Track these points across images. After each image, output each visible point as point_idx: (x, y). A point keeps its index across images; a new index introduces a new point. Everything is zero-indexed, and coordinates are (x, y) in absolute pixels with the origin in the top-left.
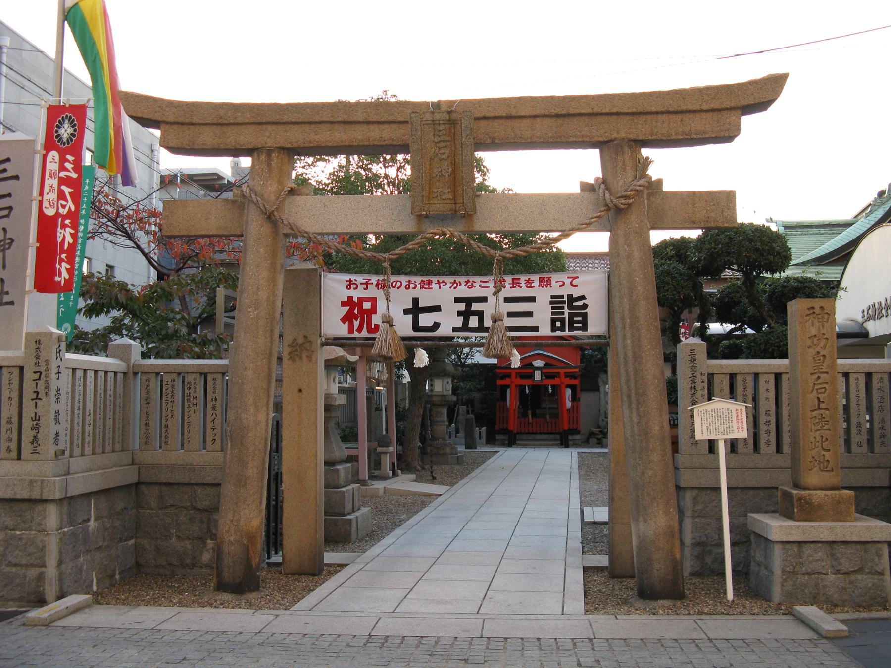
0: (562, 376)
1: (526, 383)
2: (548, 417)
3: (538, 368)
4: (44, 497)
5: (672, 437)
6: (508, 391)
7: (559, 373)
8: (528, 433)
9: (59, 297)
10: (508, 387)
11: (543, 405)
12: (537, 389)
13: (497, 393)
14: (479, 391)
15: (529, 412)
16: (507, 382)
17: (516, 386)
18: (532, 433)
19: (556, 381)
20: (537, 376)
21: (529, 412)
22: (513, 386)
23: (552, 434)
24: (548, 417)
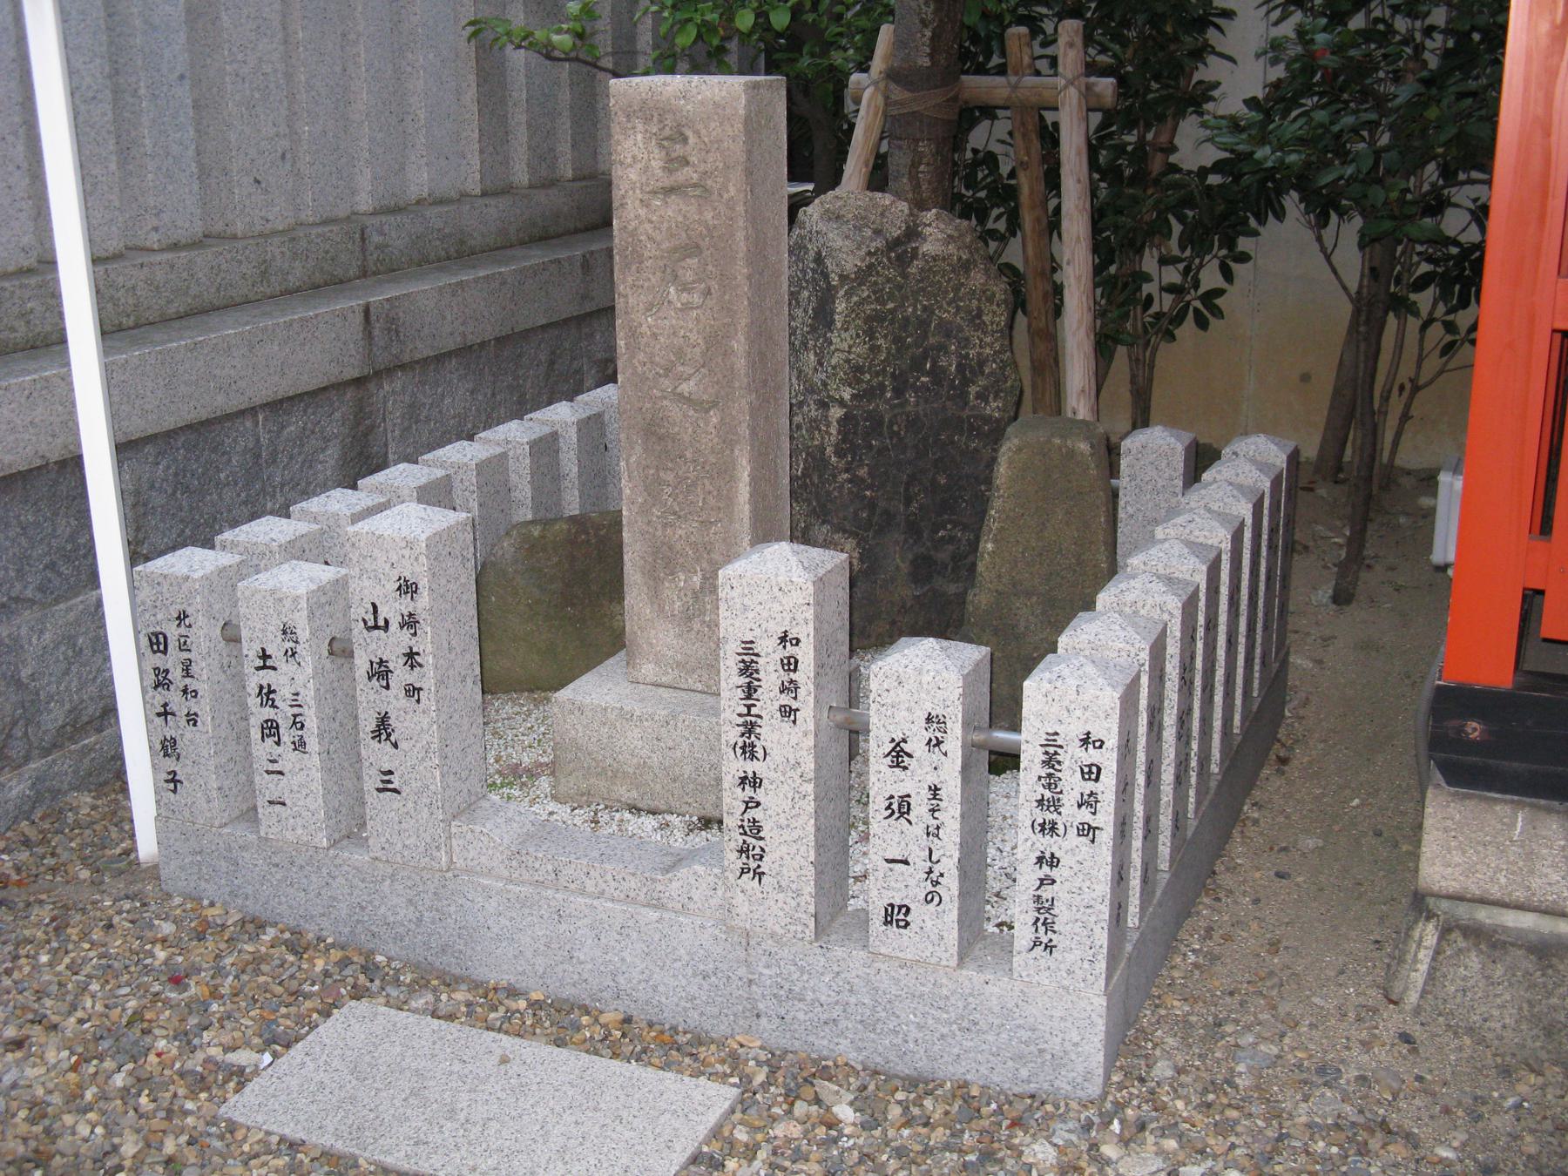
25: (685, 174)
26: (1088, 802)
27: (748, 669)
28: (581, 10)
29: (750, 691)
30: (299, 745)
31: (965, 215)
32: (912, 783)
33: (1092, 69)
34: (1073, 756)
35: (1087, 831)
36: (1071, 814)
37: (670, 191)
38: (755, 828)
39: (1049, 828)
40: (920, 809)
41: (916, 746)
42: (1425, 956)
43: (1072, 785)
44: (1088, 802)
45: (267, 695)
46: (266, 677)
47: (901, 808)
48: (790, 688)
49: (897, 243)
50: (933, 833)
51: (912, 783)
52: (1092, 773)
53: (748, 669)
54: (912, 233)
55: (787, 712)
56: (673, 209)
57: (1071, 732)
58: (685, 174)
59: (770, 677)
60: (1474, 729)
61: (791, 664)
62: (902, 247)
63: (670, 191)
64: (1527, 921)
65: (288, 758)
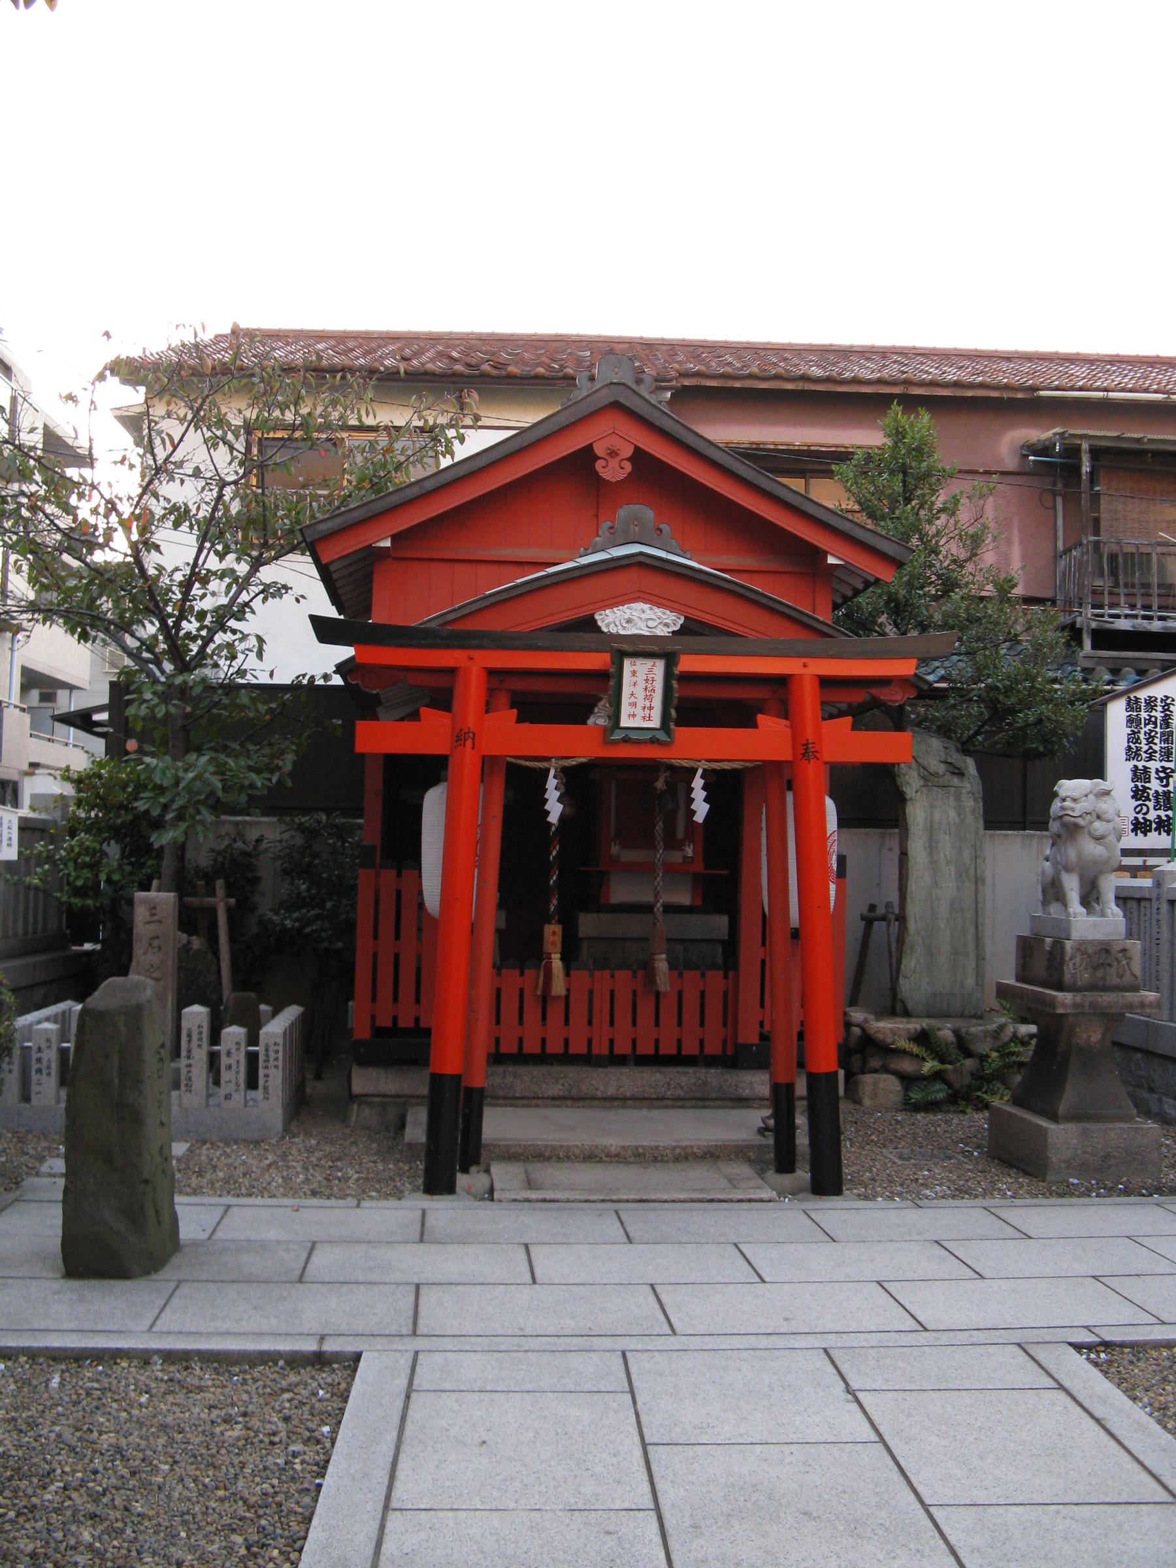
0: (808, 699)
1: (562, 745)
2: (662, 964)
3: (642, 647)
4: (414, 1396)
5: (736, 968)
6: (434, 803)
7: (781, 682)
8: (543, 1058)
9: (100, 709)
10: (431, 769)
11: (621, 892)
12: (625, 789)
13: (368, 828)
14: (272, 803)
15: (553, 933)
16: (426, 735)
17: (488, 763)
18: (567, 1058)
19: (767, 740)
20: (641, 699)
21: (553, 933)
22: (466, 764)
23: (679, 1060)
24: (662, 964)
25: (155, 918)
26: (276, 1059)
27: (189, 1036)
28: (1050, 903)
29: (189, 1041)
30: (49, 1074)
31: (1137, 560)
32: (232, 1061)
33: (228, 896)
34: (272, 1048)
35: (276, 1067)
36: (272, 1063)
37: (149, 923)
38: (190, 1079)
39: (267, 1067)
40: (234, 1067)
41: (233, 1050)
42: (355, 1113)
43: (272, 1055)
44: (276, 1059)
45: (39, 1060)
46: (39, 1055)
47: (229, 1067)
48: (200, 1039)
49: (185, 946)
50: (237, 1073)
51: (232, 1061)
52: (277, 1052)
53: (189, 1036)
54: (189, 942)
55: (200, 1046)
56: (152, 927)
57: (271, 1042)
58: (155, 918)
59: (195, 1037)
60: (362, 1050)
61: (200, 1033)
62: (186, 948)
63: (149, 923)
64: (378, 1099)
65: (44, 1078)
